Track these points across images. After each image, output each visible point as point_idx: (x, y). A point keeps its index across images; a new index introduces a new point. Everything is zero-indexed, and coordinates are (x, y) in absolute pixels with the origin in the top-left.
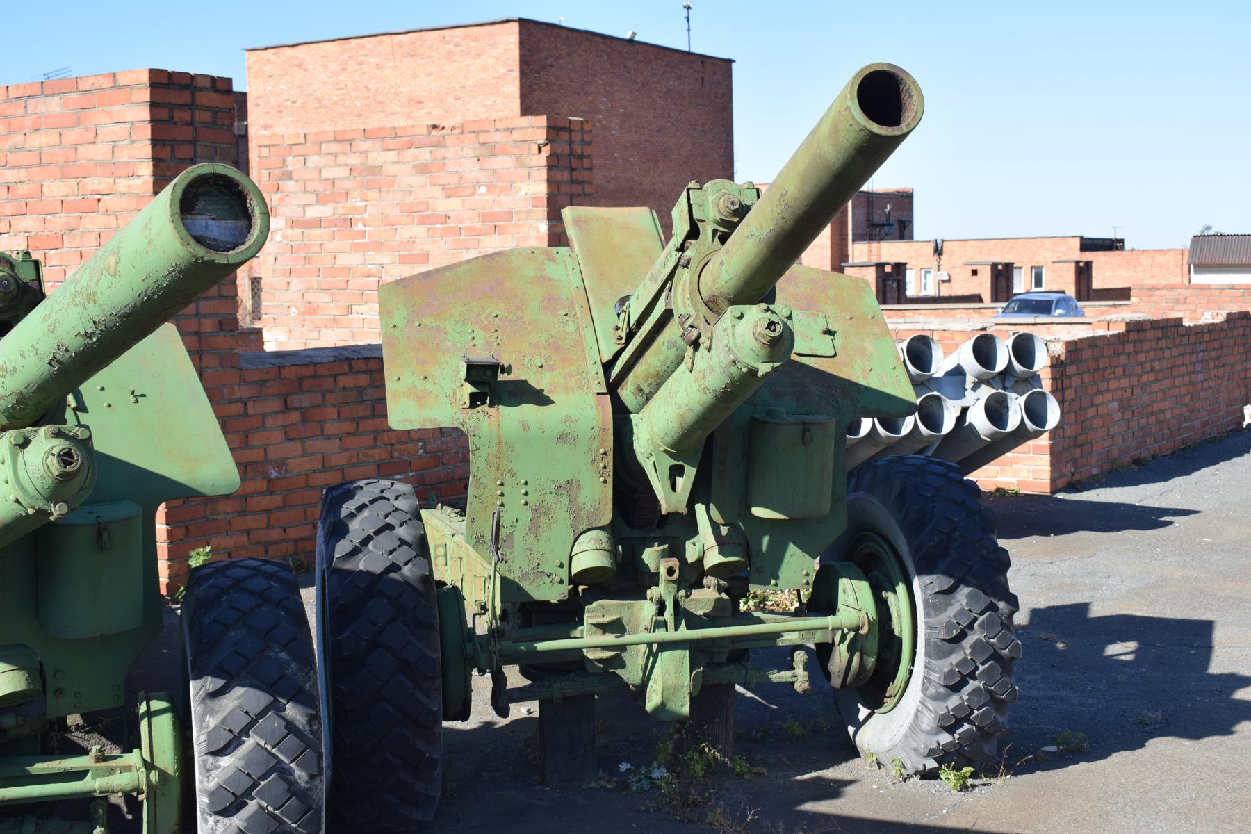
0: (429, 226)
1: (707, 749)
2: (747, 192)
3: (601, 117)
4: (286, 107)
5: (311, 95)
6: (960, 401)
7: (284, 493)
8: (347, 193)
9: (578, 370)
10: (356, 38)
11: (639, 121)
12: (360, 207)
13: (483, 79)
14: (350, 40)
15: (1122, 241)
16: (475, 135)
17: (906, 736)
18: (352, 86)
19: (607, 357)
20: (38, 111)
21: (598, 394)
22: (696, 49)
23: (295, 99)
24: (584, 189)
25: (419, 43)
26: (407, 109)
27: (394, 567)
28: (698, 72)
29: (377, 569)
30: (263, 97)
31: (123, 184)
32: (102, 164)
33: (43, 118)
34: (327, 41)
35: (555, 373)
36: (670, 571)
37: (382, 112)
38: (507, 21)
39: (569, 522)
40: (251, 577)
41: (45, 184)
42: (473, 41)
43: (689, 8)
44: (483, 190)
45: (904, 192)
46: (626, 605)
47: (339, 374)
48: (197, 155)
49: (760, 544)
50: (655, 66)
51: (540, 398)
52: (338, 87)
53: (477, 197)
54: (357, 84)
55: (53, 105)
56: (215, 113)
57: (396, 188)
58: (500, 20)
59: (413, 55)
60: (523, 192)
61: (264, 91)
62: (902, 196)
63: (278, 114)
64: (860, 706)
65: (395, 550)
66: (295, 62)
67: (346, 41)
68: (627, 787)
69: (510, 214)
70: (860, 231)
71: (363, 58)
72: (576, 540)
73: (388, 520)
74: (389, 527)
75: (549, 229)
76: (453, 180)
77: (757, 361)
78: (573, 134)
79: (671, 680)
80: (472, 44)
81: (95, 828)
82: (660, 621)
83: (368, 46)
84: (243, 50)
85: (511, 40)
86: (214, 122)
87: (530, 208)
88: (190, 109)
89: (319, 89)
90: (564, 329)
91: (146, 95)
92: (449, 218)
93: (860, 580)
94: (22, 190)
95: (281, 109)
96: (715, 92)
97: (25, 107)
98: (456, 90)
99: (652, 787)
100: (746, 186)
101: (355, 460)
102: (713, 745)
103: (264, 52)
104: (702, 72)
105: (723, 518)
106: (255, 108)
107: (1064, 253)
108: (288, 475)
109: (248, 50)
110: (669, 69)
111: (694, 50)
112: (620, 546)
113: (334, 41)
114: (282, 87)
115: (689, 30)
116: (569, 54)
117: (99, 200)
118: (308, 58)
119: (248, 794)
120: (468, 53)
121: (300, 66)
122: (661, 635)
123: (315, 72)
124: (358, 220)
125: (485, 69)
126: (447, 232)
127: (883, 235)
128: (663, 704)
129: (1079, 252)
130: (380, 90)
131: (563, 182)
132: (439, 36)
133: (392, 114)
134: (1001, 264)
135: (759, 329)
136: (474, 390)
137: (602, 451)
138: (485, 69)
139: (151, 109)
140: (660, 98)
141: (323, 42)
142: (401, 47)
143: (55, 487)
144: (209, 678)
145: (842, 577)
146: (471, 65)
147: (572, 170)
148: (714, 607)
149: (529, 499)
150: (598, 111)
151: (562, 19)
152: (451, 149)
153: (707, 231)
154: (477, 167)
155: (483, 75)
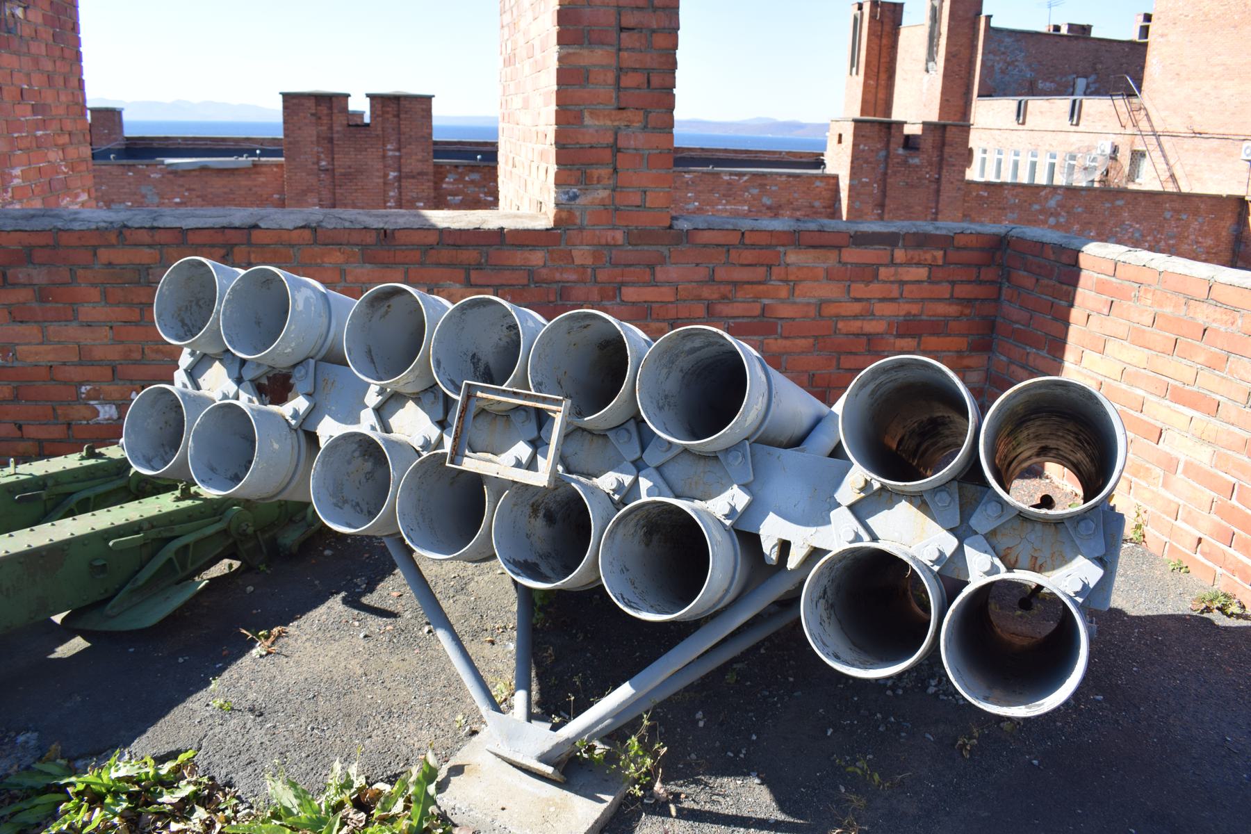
5: (1200, 10)
6: (812, 530)
7: (15, 384)
47: (100, 246)
101: (137, 356)
108: (16, 364)
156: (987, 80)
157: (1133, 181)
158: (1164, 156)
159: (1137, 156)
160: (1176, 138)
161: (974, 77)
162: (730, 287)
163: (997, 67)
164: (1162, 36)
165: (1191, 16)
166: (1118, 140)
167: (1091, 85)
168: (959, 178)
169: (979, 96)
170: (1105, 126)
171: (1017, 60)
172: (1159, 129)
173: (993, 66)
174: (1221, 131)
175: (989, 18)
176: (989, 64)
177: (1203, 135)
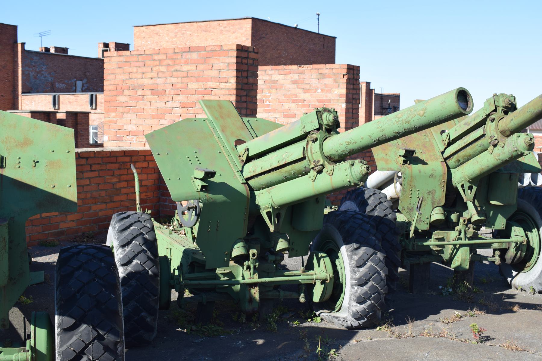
0: (296, 104)
1: (465, 283)
2: (511, 97)
3: (283, 59)
8: (263, 90)
9: (433, 154)
11: (298, 62)
12: (268, 96)
13: (235, 42)
14: (179, 24)
16: (317, 70)
17: (537, 279)
18: (179, 43)
20: (187, 57)
21: (442, 162)
22: (322, 32)
24: (357, 92)
25: (208, 26)
27: (386, 215)
28: (322, 42)
29: (382, 215)
30: (140, 46)
31: (223, 85)
32: (214, 78)
33: (189, 60)
34: (169, 24)
35: (426, 154)
38: (247, 18)
39: (431, 204)
40: (355, 214)
41: (189, 84)
42: (232, 26)
43: (319, 15)
44: (319, 91)
45: (396, 95)
46: (445, 232)
48: (248, 76)
49: (490, 214)
50: (305, 39)
51: (424, 163)
52: (173, 43)
54: (182, 42)
55: (195, 55)
56: (254, 61)
57: (283, 89)
58: (244, 18)
60: (336, 92)
61: (141, 44)
62: (395, 96)
64: (513, 271)
65: (386, 210)
66: (155, 32)
68: (442, 294)
70: (377, 111)
71: (184, 32)
72: (433, 210)
73: (141, 231)
74: (381, 203)
75: (346, 106)
76: (307, 87)
77: (524, 150)
78: (354, 71)
79: (464, 257)
80: (231, 27)
81: (301, 294)
82: (460, 238)
83: (186, 26)
85: (248, 26)
86: (253, 64)
87: (339, 98)
88: (247, 59)
89: (165, 44)
90: (426, 140)
91: (235, 54)
92: (305, 101)
93: (520, 227)
94: (179, 86)
96: (329, 51)
97: (182, 56)
99: (449, 295)
100: (511, 95)
102: (467, 282)
103: (142, 27)
104: (324, 42)
105: (479, 204)
109: (135, 27)
110: (311, 40)
112: (446, 213)
113: (172, 24)
114: (149, 42)
115: (318, 24)
116: (271, 33)
117: (212, 90)
118: (160, 31)
119: (369, 280)
120: (230, 31)
121: (157, 34)
122: (460, 242)
123: (164, 37)
124: (267, 100)
126: (304, 106)
127: (387, 113)
128: (461, 265)
131: (351, 89)
132: (217, 23)
135: (527, 140)
136: (404, 159)
137: (443, 181)
139: (236, 59)
140: (307, 52)
143: (362, 177)
144: (355, 244)
145: (513, 226)
146: (231, 36)
147: (354, 84)
148: (473, 234)
149: (419, 196)
150: (282, 57)
151: (269, 18)
152: (307, 75)
153: (500, 110)
154: (317, 82)
156: (26, 83)
161: (17, 81)
163: (32, 74)
167: (85, 85)
168: (87, 142)
169: (22, 93)
171: (42, 71)
173: (29, 74)
175: (23, 44)
176: (27, 73)
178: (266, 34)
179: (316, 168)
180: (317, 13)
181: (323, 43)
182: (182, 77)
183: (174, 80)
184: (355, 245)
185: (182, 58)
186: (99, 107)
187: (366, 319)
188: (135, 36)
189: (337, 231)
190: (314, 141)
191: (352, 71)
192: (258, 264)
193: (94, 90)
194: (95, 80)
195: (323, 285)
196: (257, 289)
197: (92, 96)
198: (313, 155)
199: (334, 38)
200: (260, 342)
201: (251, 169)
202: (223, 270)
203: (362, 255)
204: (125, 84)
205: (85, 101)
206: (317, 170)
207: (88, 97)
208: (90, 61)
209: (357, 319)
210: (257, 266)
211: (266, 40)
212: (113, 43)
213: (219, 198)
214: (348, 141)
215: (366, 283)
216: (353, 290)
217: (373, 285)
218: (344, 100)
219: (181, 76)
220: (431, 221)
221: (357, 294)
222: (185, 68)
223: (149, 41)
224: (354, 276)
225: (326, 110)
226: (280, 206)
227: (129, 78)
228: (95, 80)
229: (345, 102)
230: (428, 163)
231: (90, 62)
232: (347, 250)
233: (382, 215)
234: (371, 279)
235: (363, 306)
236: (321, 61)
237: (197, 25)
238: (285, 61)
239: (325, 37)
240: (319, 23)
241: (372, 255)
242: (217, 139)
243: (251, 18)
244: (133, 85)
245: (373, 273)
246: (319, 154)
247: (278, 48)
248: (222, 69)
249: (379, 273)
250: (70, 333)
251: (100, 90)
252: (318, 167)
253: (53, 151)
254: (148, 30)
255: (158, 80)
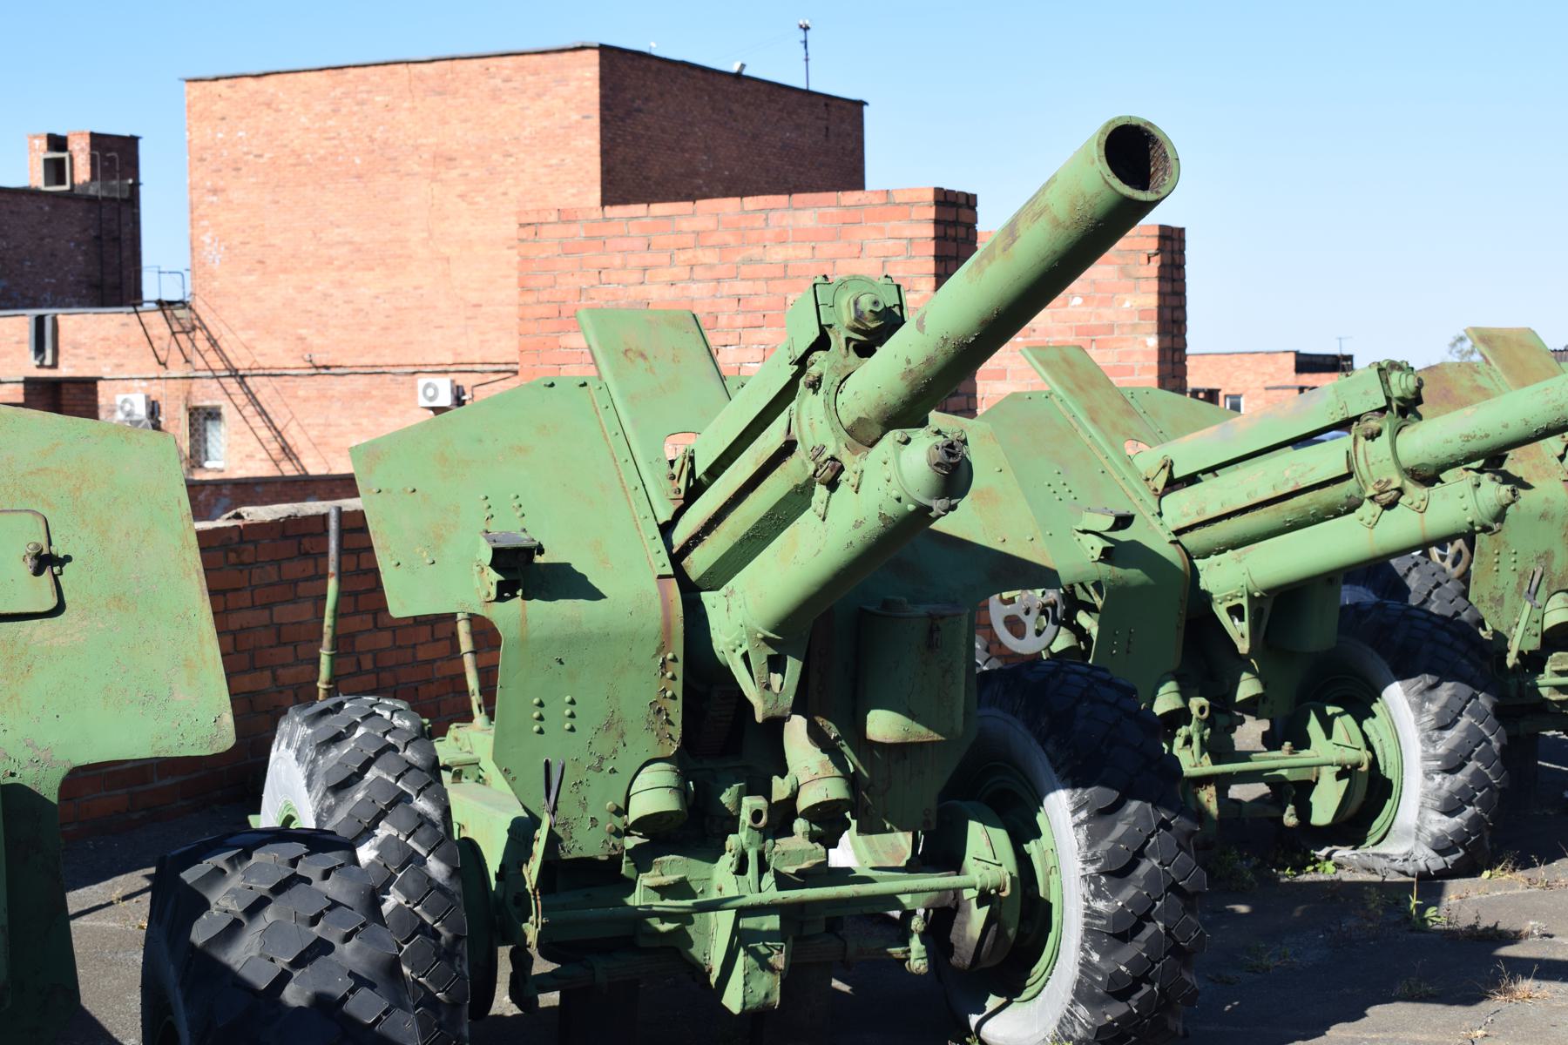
3: (701, 182)
4: (246, 163)
10: (355, 66)
13: (545, 128)
14: (345, 70)
15: (1350, 358)
18: (349, 135)
19: (665, 516)
20: (784, 224)
23: (259, 152)
25: (449, 76)
26: (431, 169)
27: (1457, 614)
28: (822, 119)
30: (210, 148)
33: (791, 232)
34: (310, 71)
36: (756, 816)
37: (393, 172)
38: (583, 48)
42: (533, 75)
43: (806, 28)
52: (326, 135)
53: (1069, 309)
58: (572, 46)
59: (441, 93)
60: (1127, 305)
61: (213, 139)
63: (234, 173)
67: (339, 71)
69: (1110, 328)
71: (365, 96)
80: (530, 79)
84: (180, 79)
85: (588, 75)
89: (298, 137)
91: (931, 213)
92: (1034, 331)
94: (758, 302)
95: (239, 166)
96: (843, 148)
97: (766, 219)
98: (506, 144)
103: (214, 83)
104: (827, 119)
106: (198, 164)
107: (1272, 376)
110: (785, 115)
111: (814, 87)
113: (321, 70)
114: (240, 134)
115: (807, 60)
116: (661, 95)
118: (281, 94)
120: (524, 92)
121: (268, 105)
123: (292, 113)
125: (548, 114)
129: (1294, 374)
130: (391, 140)
132: (481, 66)
133: (408, 175)
134: (1203, 390)
138: (548, 114)
139: (935, 227)
141: (305, 71)
142: (422, 81)
144: (1427, 676)
146: (528, 108)
153: (838, 339)
155: (545, 123)
157: (201, 466)
158: (263, 413)
159: (202, 418)
160: (278, 379)
162: (1344, 441)
164: (215, 191)
165: (267, 155)
166: (156, 390)
170: (119, 366)
172: (242, 365)
174: (367, 360)
177: (332, 371)
178: (647, 100)
179: (1383, 496)
180: (801, 23)
181: (825, 122)
182: (767, 279)
183: (741, 287)
184: (1429, 679)
185: (767, 225)
186: (66, 359)
187: (1462, 852)
188: (189, 111)
189: (1370, 650)
190: (1373, 436)
191: (1168, 243)
192: (1208, 731)
193: (27, 302)
194: (29, 263)
195: (986, 909)
196: (1212, 789)
197: (40, 321)
198: (1371, 467)
199: (860, 104)
200: (1243, 909)
201: (1183, 506)
202: (658, 873)
203: (1449, 700)
204: (586, 300)
205: (16, 339)
206: (1385, 502)
207: (27, 327)
208: (8, 199)
209: (1442, 852)
210: (1206, 738)
211: (646, 120)
212: (82, 134)
213: (1134, 575)
214: (1466, 433)
215: (1460, 767)
216: (1431, 784)
217: (1478, 769)
218: (1152, 324)
219: (765, 275)
220: (1546, 627)
221: (1444, 792)
222: (778, 254)
223: (242, 130)
224: (1432, 751)
225: (1394, 366)
226: (1265, 591)
227: (601, 283)
228: (29, 263)
229: (1155, 329)
230: (1532, 484)
231: (7, 202)
232: (1406, 693)
233: (1450, 614)
234: (1473, 756)
235: (1457, 819)
236: (820, 183)
237: (410, 72)
238: (707, 186)
239: (829, 102)
240: (807, 54)
241: (1468, 702)
242: (1088, 441)
243: (597, 45)
244: (614, 303)
245: (1477, 742)
246: (1391, 465)
247: (683, 143)
248: (890, 254)
249: (1489, 742)
250: (1110, 818)
251: (45, 300)
252: (1388, 494)
253: (414, 491)
254: (236, 92)
255: (694, 287)
